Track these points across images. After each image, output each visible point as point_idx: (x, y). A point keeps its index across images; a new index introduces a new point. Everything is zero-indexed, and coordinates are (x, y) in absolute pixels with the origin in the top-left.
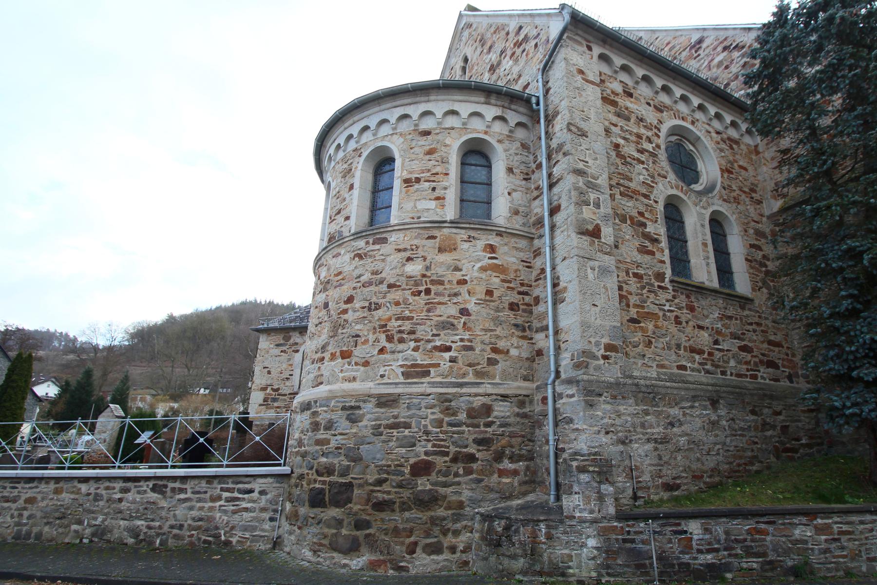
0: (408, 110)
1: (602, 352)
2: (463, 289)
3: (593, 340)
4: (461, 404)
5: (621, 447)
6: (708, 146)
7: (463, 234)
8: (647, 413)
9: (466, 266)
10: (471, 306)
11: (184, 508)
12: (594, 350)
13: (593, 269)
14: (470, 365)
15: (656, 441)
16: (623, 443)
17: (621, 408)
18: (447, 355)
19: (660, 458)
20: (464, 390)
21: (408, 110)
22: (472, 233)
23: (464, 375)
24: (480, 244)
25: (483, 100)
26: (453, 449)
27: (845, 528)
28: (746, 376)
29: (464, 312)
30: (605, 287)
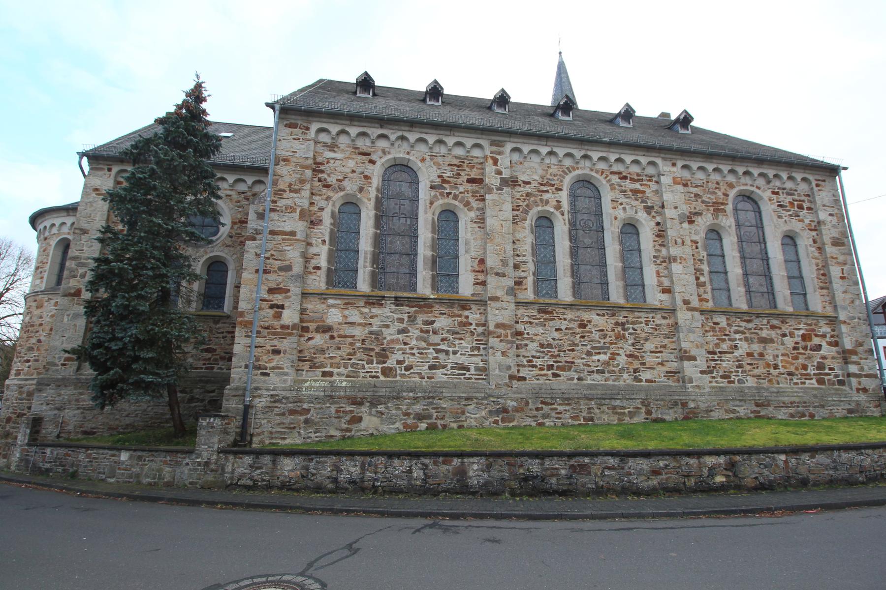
0: (574, 152)
1: (62, 362)
2: (41, 328)
3: (57, 356)
4: (25, 389)
5: (56, 412)
6: (371, 205)
7: (46, 297)
8: (81, 394)
9: (45, 314)
10: (42, 338)
11: (785, 414)
12: (57, 361)
13: (68, 315)
14: (35, 369)
15: (84, 409)
16: (59, 409)
17: (63, 392)
18: (27, 364)
19: (85, 417)
20: (28, 382)
21: (574, 152)
22: (50, 296)
23: (32, 375)
24: (53, 302)
25: (65, 214)
26: (19, 411)
27: (96, 456)
28: (202, 368)
29: (39, 341)
30: (75, 325)
